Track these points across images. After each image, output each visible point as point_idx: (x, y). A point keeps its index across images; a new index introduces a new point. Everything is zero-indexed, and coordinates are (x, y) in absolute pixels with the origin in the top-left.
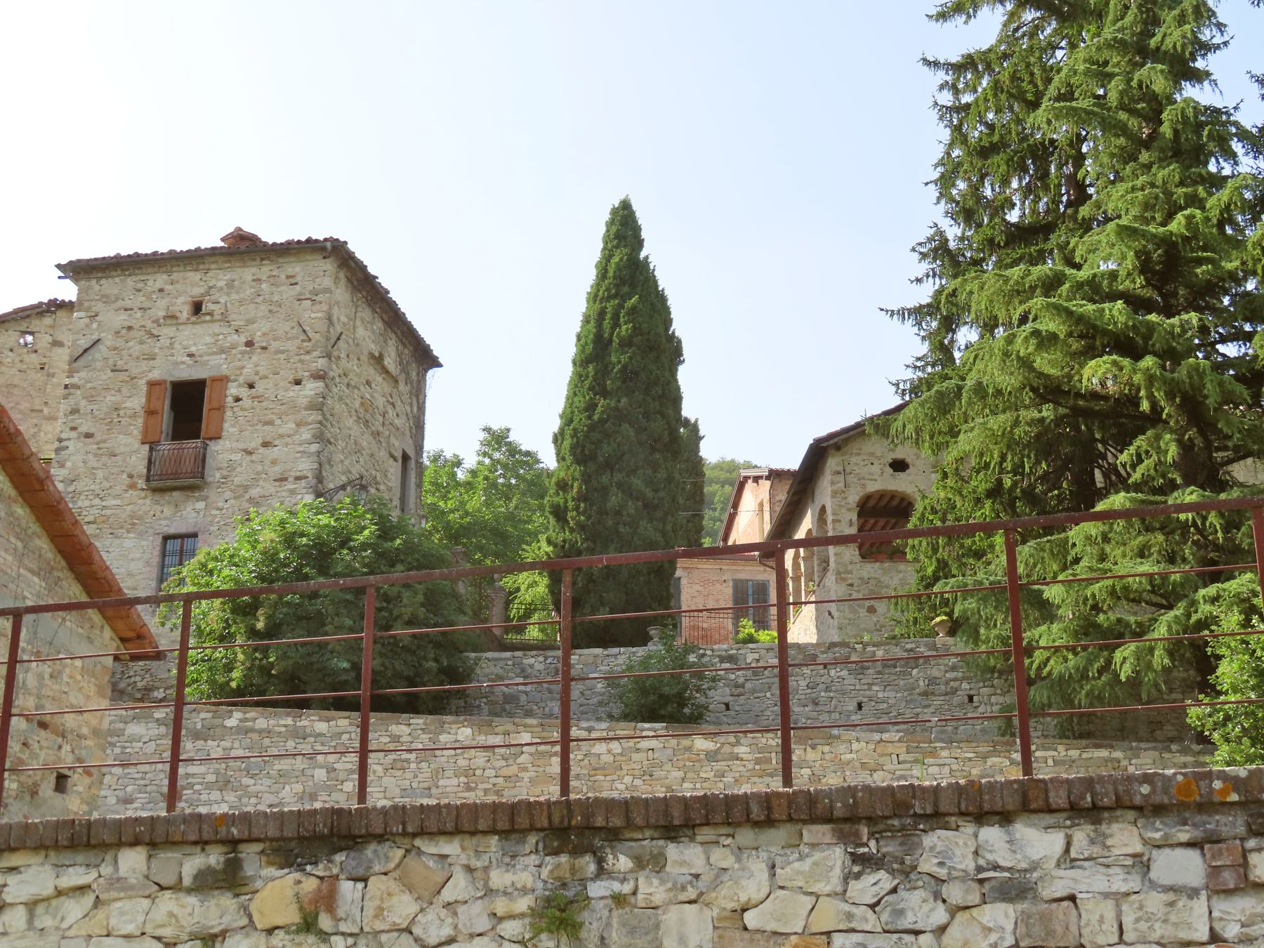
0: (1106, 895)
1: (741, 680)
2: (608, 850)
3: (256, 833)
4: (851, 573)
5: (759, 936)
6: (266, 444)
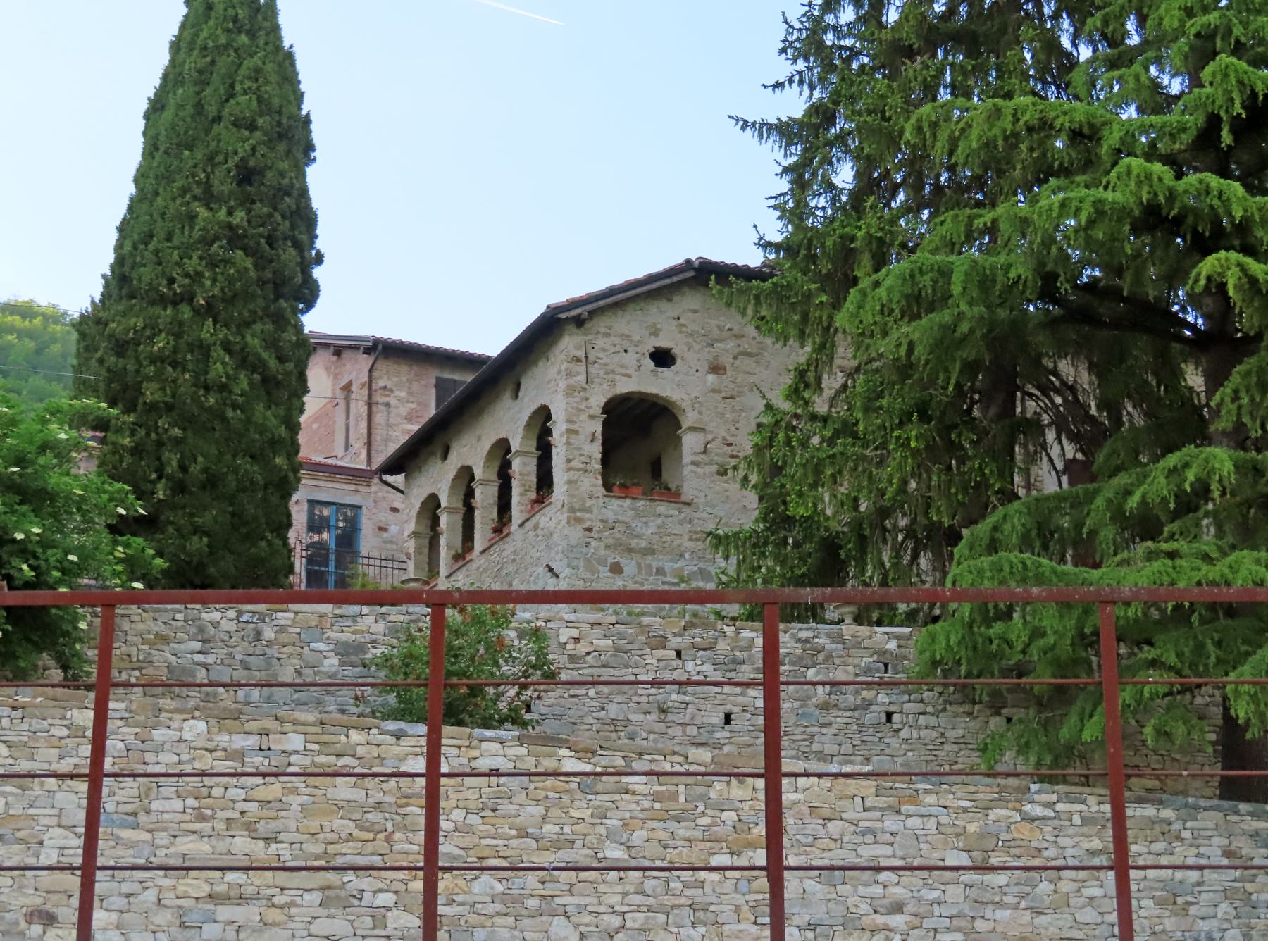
4: (589, 511)
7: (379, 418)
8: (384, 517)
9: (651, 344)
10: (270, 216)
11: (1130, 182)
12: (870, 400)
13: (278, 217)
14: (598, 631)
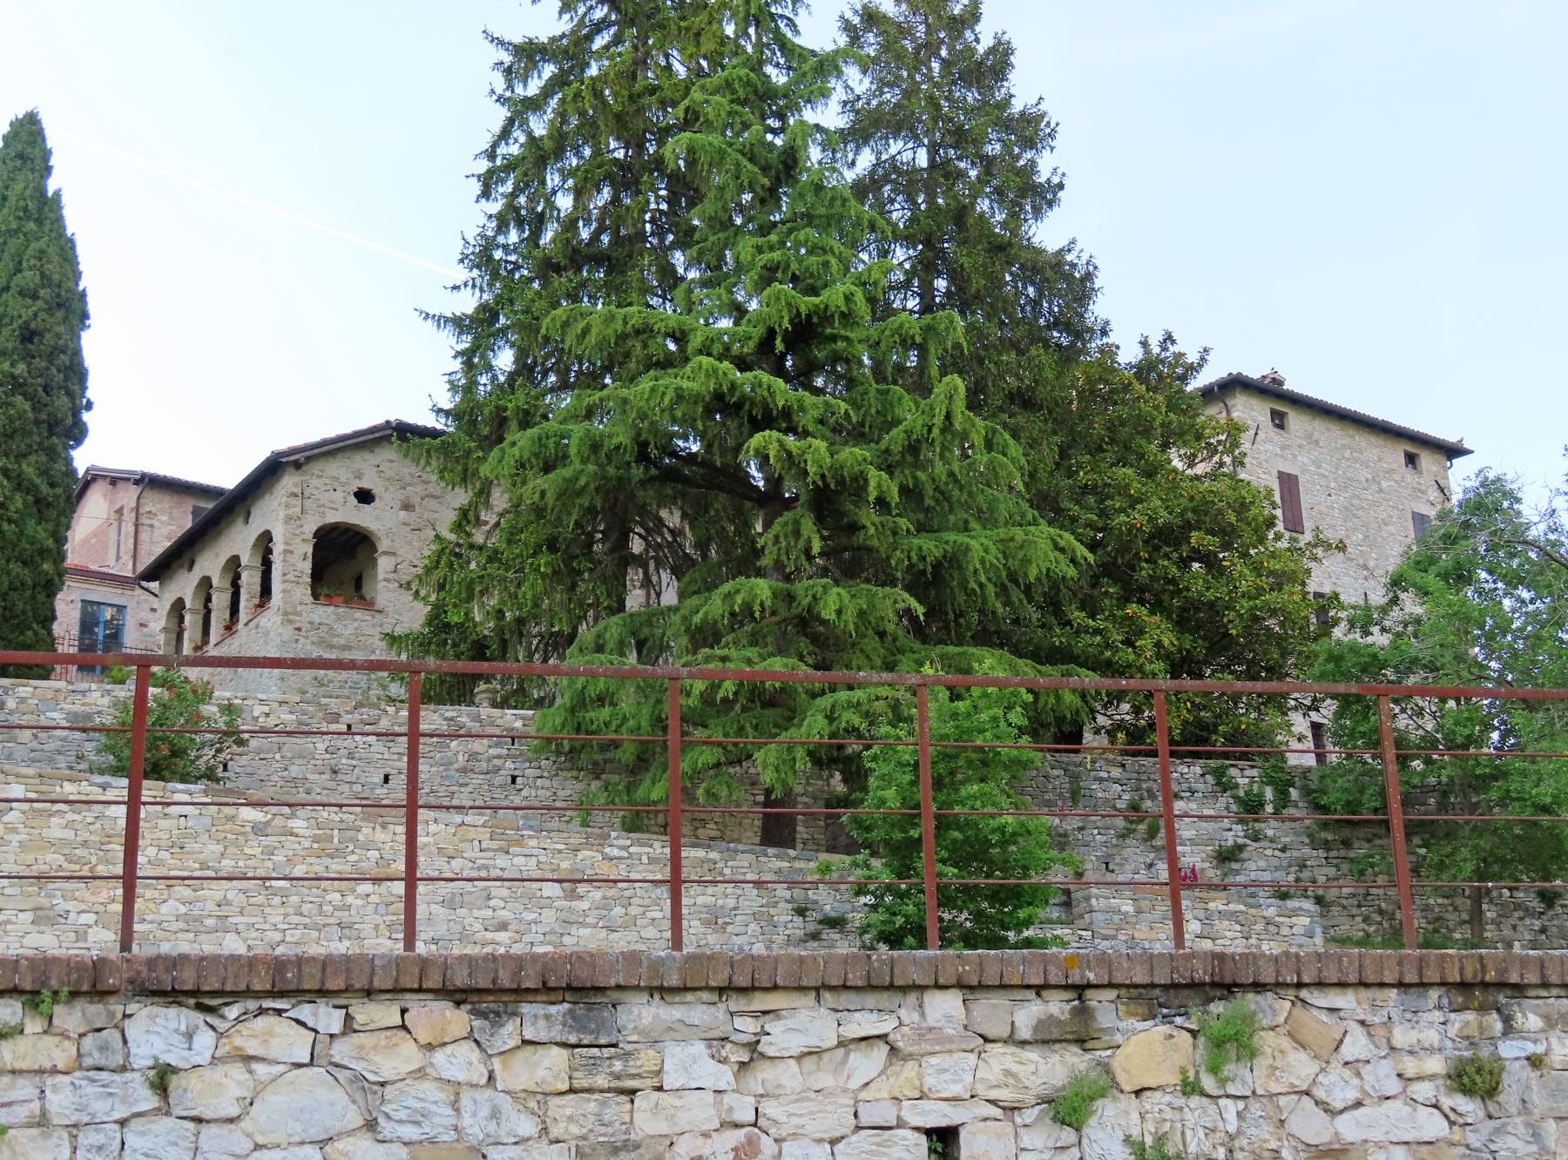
2: (1516, 1008)
3: (1119, 978)
4: (299, 614)
7: (144, 536)
8: (145, 615)
9: (356, 485)
10: (48, 369)
11: (696, 377)
12: (512, 534)
13: (54, 370)
14: (285, 708)
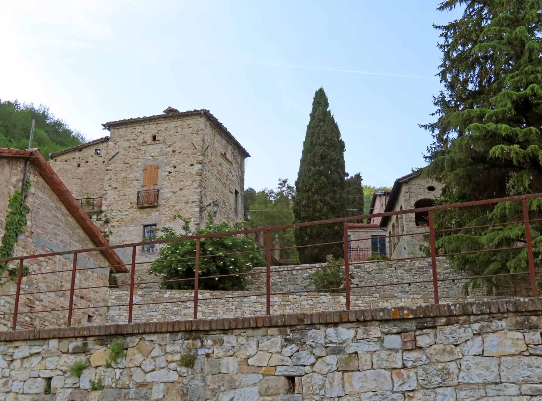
0: (368, 352)
1: (363, 275)
3: (92, 334)
5: (252, 368)
6: (181, 189)
9: (427, 185)
13: (332, 166)
